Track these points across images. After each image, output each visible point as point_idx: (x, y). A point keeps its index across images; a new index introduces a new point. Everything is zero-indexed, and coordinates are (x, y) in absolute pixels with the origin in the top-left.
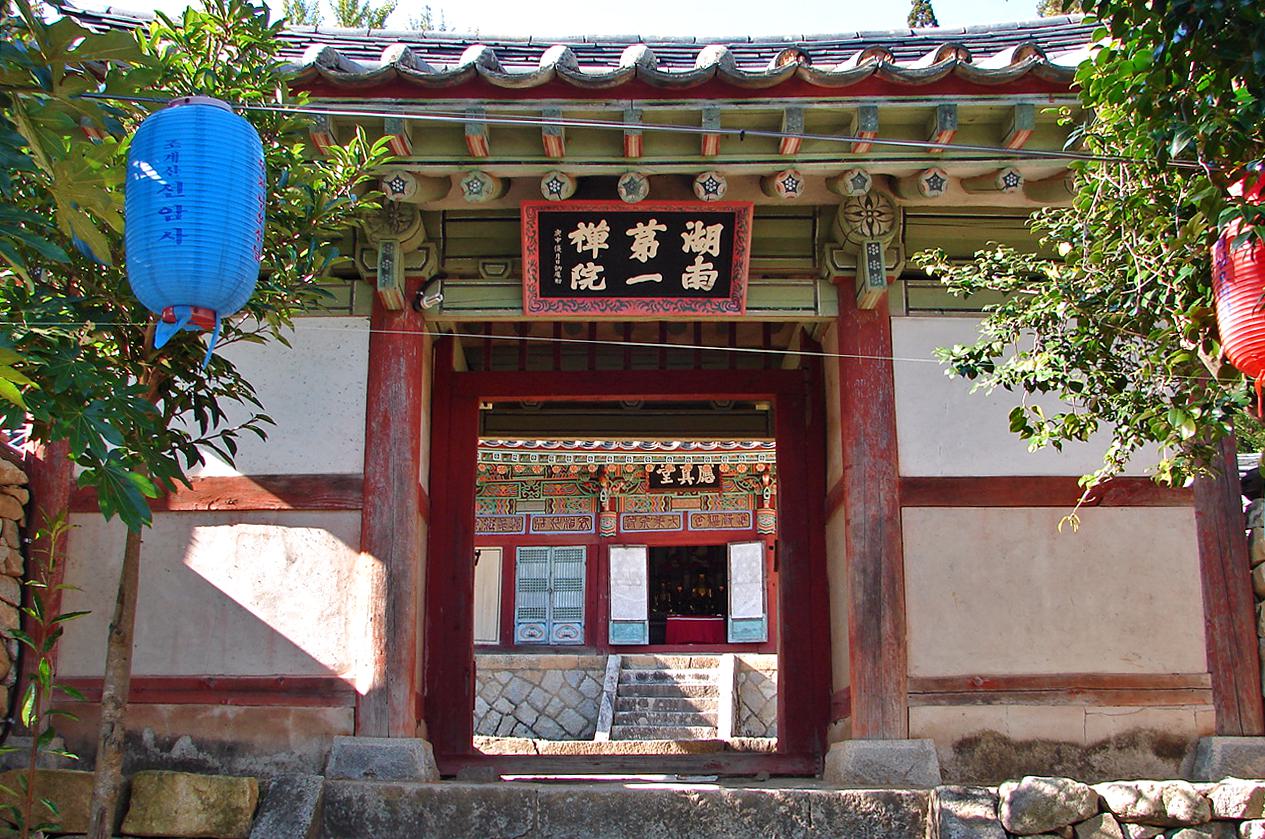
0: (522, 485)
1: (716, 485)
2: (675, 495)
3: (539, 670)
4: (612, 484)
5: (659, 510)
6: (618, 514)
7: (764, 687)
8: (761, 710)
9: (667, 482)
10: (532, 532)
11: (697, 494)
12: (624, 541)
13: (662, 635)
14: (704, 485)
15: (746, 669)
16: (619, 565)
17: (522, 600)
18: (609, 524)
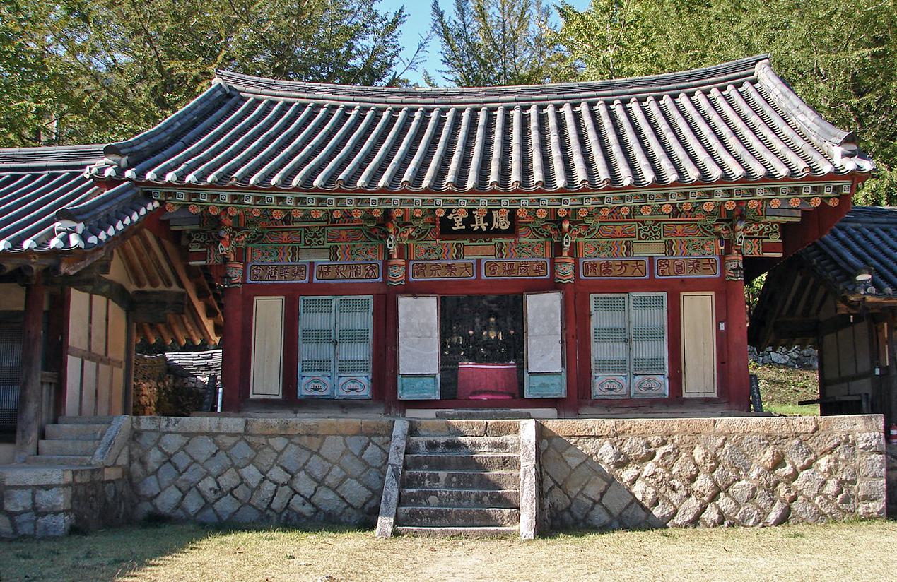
1: (512, 232)
2: (467, 242)
3: (317, 436)
5: (450, 258)
6: (407, 262)
10: (315, 280)
12: (414, 290)
13: (453, 394)
16: (408, 315)
17: (306, 351)
18: (398, 273)
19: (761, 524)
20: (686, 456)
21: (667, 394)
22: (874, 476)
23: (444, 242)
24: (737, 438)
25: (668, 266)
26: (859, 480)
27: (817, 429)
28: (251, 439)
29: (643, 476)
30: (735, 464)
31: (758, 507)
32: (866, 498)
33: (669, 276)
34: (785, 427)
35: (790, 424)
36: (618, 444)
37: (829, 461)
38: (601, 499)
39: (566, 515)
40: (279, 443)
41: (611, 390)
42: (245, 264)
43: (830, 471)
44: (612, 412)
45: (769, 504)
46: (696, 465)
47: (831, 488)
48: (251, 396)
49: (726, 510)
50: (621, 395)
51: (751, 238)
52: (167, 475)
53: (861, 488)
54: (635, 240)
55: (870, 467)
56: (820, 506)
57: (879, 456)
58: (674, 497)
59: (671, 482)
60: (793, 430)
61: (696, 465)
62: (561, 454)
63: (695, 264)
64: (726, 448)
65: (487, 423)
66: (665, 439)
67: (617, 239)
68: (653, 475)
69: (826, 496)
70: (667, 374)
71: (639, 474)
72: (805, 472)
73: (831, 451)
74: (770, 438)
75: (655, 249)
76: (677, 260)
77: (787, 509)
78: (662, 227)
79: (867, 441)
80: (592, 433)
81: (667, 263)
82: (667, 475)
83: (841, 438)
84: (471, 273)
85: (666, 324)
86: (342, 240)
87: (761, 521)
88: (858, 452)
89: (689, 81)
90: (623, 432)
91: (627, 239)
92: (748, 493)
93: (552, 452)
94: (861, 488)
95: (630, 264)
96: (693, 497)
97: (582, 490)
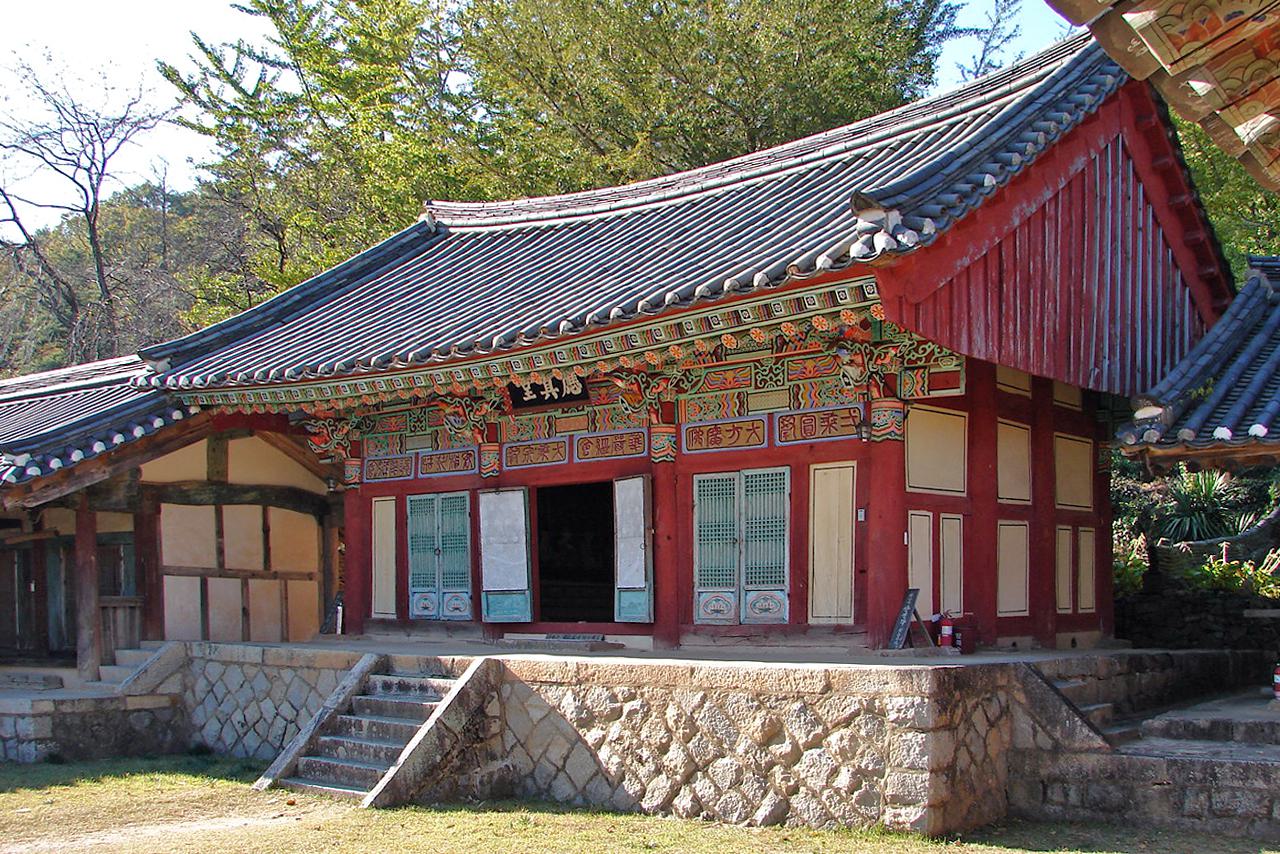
0: (756, 367)
2: (558, 414)
3: (315, 669)
4: (876, 352)
5: (542, 436)
6: (501, 446)
7: (531, 705)
8: (527, 738)
9: (530, 398)
10: (420, 476)
11: (583, 410)
12: (498, 484)
14: (571, 397)
15: (510, 679)
16: (490, 517)
19: (748, 821)
20: (656, 717)
21: (787, 619)
22: (912, 767)
23: (535, 416)
24: (719, 695)
25: (794, 426)
26: (888, 770)
27: (828, 687)
28: (267, 670)
29: (608, 739)
30: (717, 733)
31: (744, 796)
32: (898, 800)
33: (795, 439)
34: (783, 682)
35: (791, 678)
36: (582, 694)
37: (842, 739)
38: (564, 766)
39: (529, 782)
40: (287, 675)
41: (717, 611)
42: (678, 428)
43: (842, 752)
44: (718, 643)
45: (759, 795)
46: (668, 730)
47: (843, 780)
48: (374, 616)
49: (703, 797)
50: (727, 620)
51: (913, 369)
52: (210, 702)
53: (890, 784)
54: (751, 390)
55: (905, 753)
56: (828, 804)
57: (920, 736)
58: (642, 771)
59: (639, 751)
60: (794, 687)
61: (668, 730)
62: (523, 704)
63: (832, 418)
64: (705, 709)
65: (453, 660)
66: (633, 691)
67: (728, 392)
68: (618, 739)
69: (837, 791)
70: (787, 590)
71: (604, 736)
72: (810, 751)
73: (847, 722)
74: (761, 698)
75: (771, 402)
76: (805, 415)
77: (784, 805)
78: (786, 364)
79: (899, 711)
80: (554, 679)
81: (792, 421)
82: (635, 741)
83: (861, 704)
84: (761, 439)
85: (787, 514)
86: (729, 386)
87: (747, 817)
88: (888, 726)
89: (981, 94)
90: (587, 680)
91: (740, 390)
92: (730, 776)
93: (514, 701)
94: (890, 784)
95: (745, 427)
96: (663, 776)
97: (545, 752)
